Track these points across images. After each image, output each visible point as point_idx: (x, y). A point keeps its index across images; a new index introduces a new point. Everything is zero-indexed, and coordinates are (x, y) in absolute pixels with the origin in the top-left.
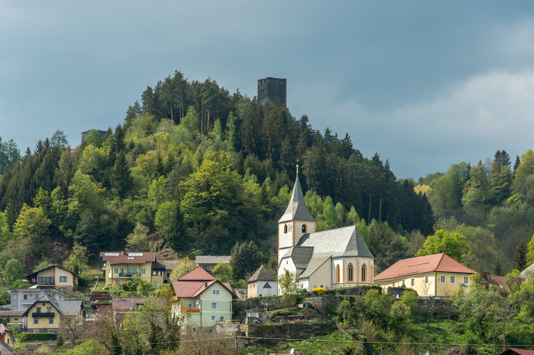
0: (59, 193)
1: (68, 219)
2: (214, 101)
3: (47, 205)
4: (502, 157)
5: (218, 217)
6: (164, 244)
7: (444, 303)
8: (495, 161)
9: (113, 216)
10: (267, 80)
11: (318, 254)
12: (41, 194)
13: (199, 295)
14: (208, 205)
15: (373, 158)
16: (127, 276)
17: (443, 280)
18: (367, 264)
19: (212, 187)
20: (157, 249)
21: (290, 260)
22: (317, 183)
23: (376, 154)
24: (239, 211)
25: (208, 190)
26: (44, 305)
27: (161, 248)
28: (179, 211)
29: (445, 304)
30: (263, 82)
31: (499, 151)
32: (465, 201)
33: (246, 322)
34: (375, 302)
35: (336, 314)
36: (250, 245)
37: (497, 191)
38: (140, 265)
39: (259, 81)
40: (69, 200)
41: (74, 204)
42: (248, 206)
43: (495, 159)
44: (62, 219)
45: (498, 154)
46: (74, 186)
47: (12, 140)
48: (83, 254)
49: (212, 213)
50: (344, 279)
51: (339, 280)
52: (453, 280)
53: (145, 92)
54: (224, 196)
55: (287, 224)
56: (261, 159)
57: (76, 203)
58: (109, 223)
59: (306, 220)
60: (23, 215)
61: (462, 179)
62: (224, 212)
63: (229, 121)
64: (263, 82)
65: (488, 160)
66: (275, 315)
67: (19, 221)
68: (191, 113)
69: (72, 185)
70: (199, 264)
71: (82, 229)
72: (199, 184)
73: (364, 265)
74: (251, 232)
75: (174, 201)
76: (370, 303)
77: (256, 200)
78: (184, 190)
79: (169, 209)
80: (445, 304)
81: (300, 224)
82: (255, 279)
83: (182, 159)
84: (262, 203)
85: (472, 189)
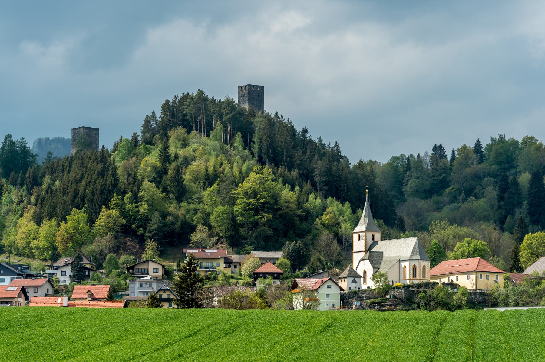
0: (130, 198)
1: (139, 220)
2: (234, 118)
3: (121, 207)
4: (438, 150)
5: (265, 220)
6: (218, 240)
7: (485, 294)
8: (432, 154)
9: (176, 217)
10: (247, 87)
11: (387, 257)
12: (115, 199)
13: (317, 289)
14: (256, 210)
15: (358, 163)
16: (205, 268)
17: (481, 277)
18: (426, 266)
19: (259, 196)
20: (213, 244)
21: (368, 262)
22: (326, 188)
23: (361, 160)
24: (279, 215)
25: (255, 197)
26: (165, 292)
27: (217, 244)
28: (233, 215)
29: (487, 296)
30: (244, 88)
31: (436, 145)
32: (406, 191)
33: (354, 308)
34: (441, 294)
35: (414, 303)
36: (298, 244)
37: (435, 182)
38: (216, 259)
39: (239, 87)
40: (139, 204)
41: (144, 208)
42: (287, 211)
43: (432, 152)
44: (134, 220)
45: (435, 147)
46: (143, 192)
47: (23, 138)
48: (156, 248)
49: (259, 216)
50: (410, 276)
51: (405, 277)
52: (488, 277)
53: (164, 105)
54: (269, 203)
55: (361, 234)
56: (290, 170)
57: (146, 206)
58: (173, 223)
59: (375, 232)
60: (102, 215)
61: (401, 170)
62: (270, 216)
63: (255, 136)
64: (244, 88)
65: (426, 153)
66: (371, 303)
67: (99, 220)
68: (219, 128)
69: (141, 192)
70: (260, 258)
71: (152, 228)
72: (248, 192)
73: (424, 266)
74: (291, 232)
75: (226, 206)
76: (438, 296)
77: (293, 206)
78: (234, 197)
79: (223, 213)
80: (487, 296)
81: (370, 235)
82: (346, 276)
83: (224, 170)
84: (299, 209)
85: (413, 179)
